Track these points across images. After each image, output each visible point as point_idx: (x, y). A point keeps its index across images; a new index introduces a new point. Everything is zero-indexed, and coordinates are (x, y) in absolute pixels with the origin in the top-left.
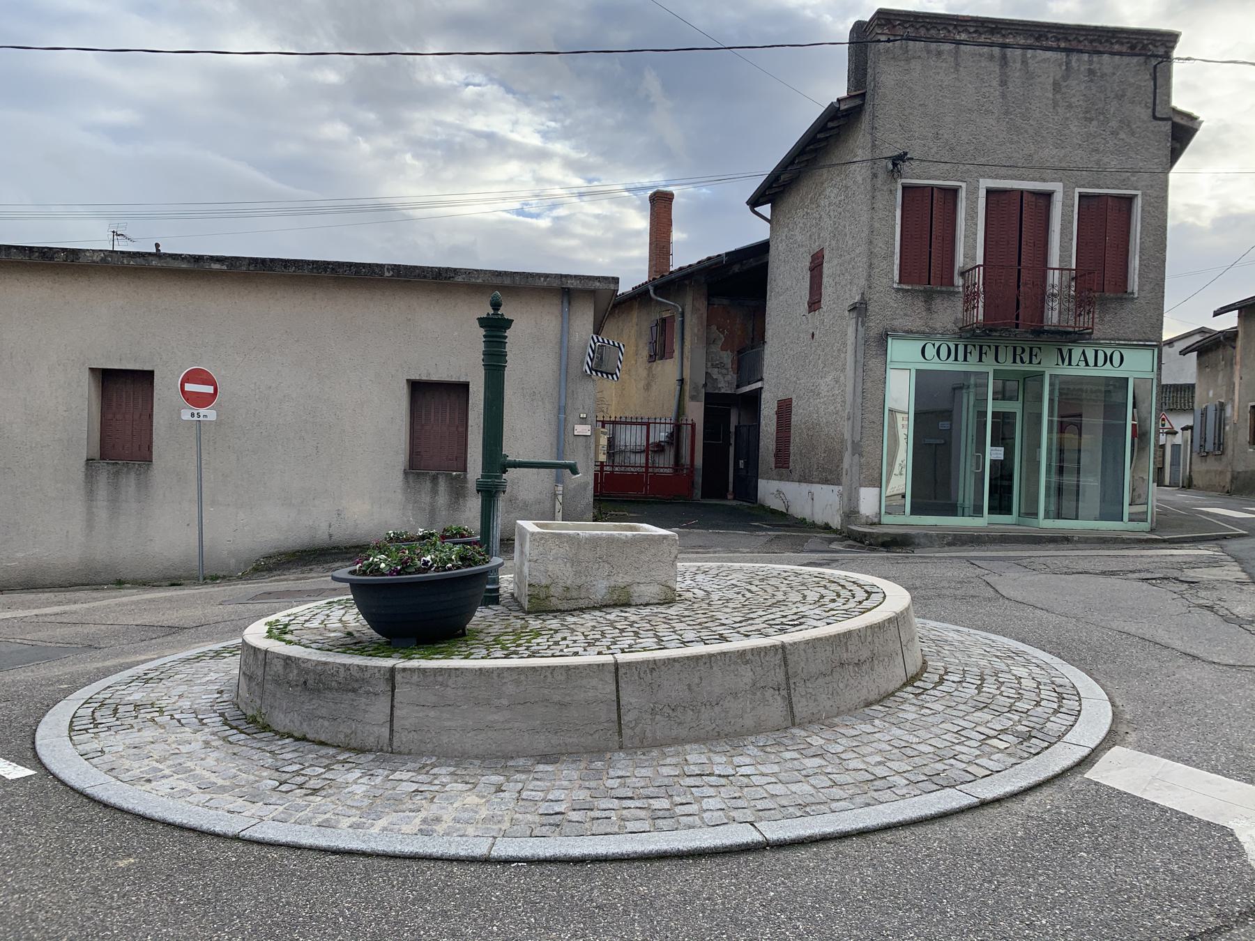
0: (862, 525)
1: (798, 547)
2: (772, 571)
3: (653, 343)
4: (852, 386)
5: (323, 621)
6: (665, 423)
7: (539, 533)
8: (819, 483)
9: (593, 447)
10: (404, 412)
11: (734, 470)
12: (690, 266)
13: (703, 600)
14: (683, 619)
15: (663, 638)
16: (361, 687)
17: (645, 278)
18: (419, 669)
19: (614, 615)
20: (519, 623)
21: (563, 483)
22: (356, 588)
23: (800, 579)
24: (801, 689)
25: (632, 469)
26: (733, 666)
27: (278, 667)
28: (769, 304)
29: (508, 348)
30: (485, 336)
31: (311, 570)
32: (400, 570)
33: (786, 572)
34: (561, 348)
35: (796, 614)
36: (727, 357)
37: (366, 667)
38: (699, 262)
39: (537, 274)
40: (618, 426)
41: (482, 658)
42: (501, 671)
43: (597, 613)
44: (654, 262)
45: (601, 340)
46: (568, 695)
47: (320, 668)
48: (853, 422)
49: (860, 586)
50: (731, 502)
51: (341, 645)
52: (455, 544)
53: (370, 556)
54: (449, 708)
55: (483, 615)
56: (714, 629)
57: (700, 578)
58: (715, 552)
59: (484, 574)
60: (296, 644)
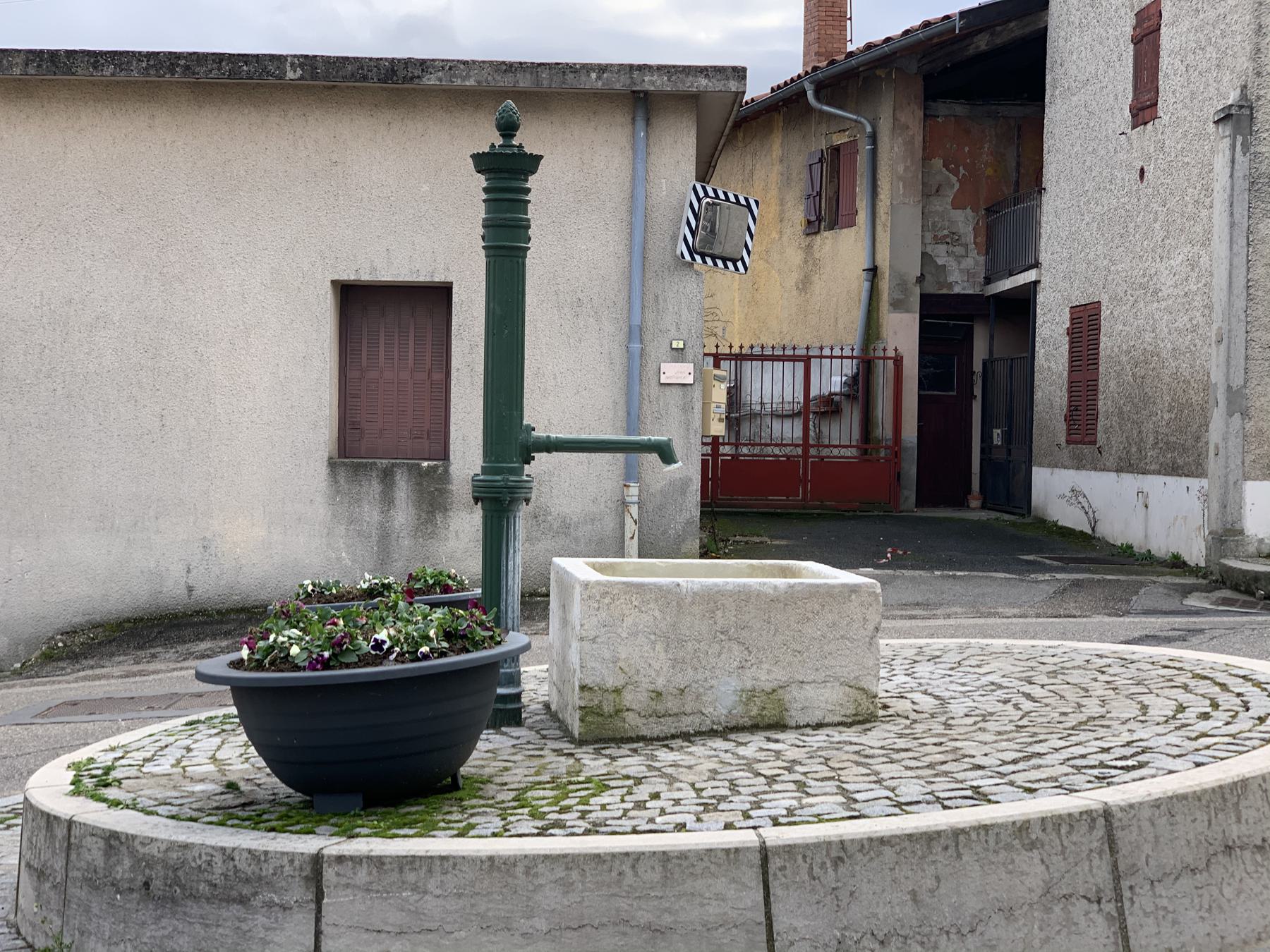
0: (1248, 558)
1: (1119, 604)
2: (1073, 655)
3: (814, 197)
4: (1225, 275)
5: (179, 761)
6: (842, 357)
7: (598, 583)
8: (1159, 473)
9: (698, 406)
10: (327, 345)
11: (983, 451)
12: (888, 40)
13: (932, 716)
14: (895, 756)
15: (857, 796)
16: (255, 894)
17: (799, 69)
18: (369, 858)
19: (753, 746)
20: (563, 764)
21: (638, 480)
22: (244, 694)
23: (1132, 671)
24: (1144, 899)
25: (777, 451)
26: (1003, 854)
27: (94, 852)
28: (1049, 112)
29: (532, 213)
30: (486, 190)
31: (154, 656)
32: (330, 659)
33: (1101, 656)
34: (632, 212)
35: (1128, 744)
36: (965, 222)
37: (266, 853)
38: (907, 32)
39: (584, 66)
40: (747, 365)
41: (494, 835)
42: (532, 863)
43: (719, 743)
44: (814, 36)
45: (711, 194)
46: (668, 910)
47: (175, 856)
48: (1229, 347)
49: (1258, 684)
50: (975, 513)
51: (217, 808)
52: (434, 605)
53: (269, 631)
54: (430, 936)
55: (491, 746)
56: (960, 776)
57: (923, 669)
58: (949, 616)
59: (490, 667)
60: (127, 807)
